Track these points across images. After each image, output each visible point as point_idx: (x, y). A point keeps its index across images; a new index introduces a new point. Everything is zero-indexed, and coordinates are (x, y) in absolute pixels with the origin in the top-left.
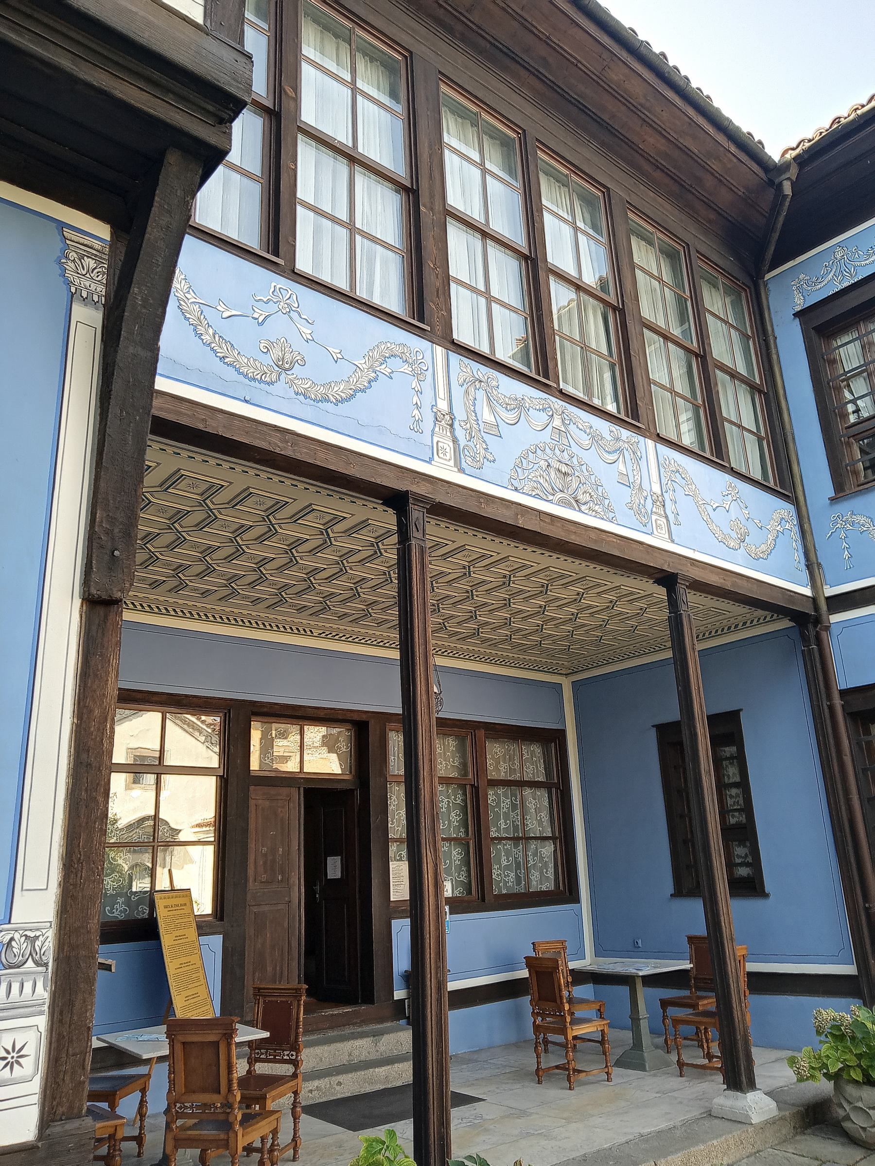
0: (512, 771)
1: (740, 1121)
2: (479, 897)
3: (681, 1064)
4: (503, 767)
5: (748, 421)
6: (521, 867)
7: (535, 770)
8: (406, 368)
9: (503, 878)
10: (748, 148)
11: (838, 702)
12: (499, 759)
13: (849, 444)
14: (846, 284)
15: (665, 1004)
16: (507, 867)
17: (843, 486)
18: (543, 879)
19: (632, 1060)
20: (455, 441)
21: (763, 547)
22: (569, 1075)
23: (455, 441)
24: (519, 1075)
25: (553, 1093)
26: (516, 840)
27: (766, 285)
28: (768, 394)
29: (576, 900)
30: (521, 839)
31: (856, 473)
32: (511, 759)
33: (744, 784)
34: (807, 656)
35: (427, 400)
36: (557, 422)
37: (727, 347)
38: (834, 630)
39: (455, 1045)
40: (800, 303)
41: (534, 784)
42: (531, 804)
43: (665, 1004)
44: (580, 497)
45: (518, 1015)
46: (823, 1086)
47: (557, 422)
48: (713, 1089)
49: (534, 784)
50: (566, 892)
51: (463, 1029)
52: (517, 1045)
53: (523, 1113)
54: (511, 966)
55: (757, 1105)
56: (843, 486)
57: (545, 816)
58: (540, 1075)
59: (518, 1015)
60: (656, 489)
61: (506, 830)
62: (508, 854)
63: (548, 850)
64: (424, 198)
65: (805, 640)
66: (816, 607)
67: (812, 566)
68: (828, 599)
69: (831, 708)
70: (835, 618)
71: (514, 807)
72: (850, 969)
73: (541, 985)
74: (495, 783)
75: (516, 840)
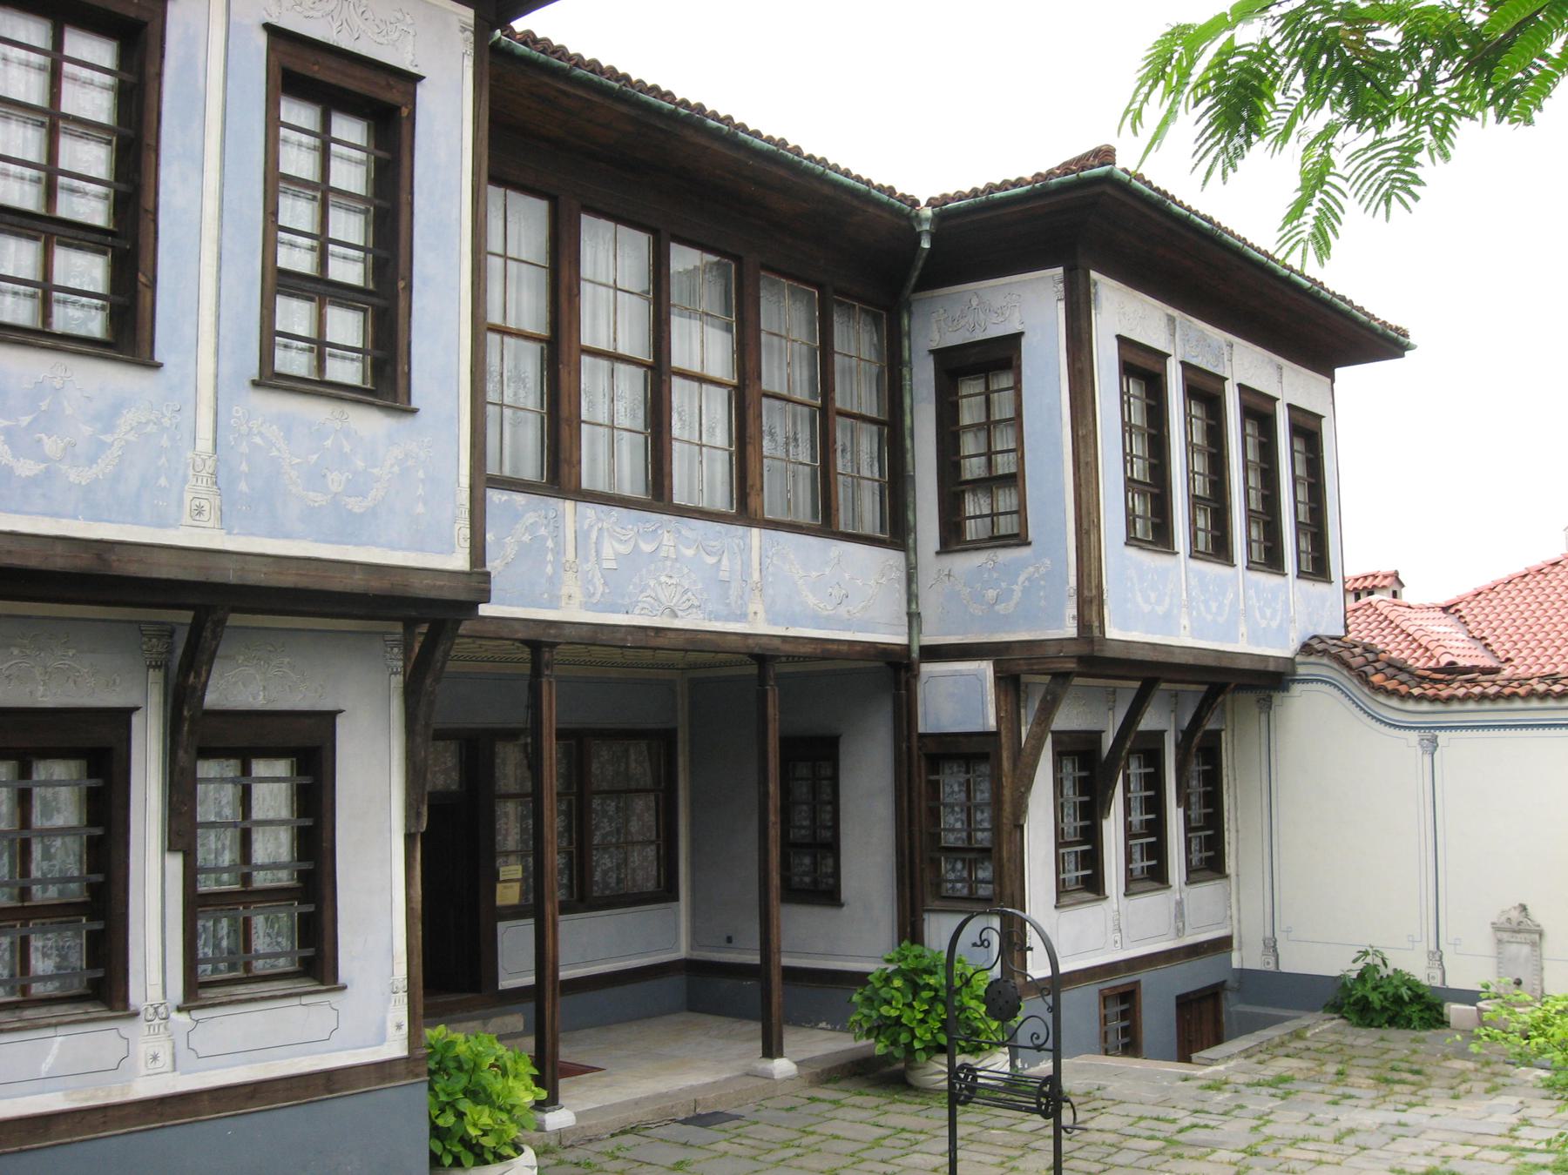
1: (768, 1077)
2: (583, 899)
17: (952, 538)
37: (857, 392)
55: (782, 1067)
56: (952, 538)
67: (913, 618)
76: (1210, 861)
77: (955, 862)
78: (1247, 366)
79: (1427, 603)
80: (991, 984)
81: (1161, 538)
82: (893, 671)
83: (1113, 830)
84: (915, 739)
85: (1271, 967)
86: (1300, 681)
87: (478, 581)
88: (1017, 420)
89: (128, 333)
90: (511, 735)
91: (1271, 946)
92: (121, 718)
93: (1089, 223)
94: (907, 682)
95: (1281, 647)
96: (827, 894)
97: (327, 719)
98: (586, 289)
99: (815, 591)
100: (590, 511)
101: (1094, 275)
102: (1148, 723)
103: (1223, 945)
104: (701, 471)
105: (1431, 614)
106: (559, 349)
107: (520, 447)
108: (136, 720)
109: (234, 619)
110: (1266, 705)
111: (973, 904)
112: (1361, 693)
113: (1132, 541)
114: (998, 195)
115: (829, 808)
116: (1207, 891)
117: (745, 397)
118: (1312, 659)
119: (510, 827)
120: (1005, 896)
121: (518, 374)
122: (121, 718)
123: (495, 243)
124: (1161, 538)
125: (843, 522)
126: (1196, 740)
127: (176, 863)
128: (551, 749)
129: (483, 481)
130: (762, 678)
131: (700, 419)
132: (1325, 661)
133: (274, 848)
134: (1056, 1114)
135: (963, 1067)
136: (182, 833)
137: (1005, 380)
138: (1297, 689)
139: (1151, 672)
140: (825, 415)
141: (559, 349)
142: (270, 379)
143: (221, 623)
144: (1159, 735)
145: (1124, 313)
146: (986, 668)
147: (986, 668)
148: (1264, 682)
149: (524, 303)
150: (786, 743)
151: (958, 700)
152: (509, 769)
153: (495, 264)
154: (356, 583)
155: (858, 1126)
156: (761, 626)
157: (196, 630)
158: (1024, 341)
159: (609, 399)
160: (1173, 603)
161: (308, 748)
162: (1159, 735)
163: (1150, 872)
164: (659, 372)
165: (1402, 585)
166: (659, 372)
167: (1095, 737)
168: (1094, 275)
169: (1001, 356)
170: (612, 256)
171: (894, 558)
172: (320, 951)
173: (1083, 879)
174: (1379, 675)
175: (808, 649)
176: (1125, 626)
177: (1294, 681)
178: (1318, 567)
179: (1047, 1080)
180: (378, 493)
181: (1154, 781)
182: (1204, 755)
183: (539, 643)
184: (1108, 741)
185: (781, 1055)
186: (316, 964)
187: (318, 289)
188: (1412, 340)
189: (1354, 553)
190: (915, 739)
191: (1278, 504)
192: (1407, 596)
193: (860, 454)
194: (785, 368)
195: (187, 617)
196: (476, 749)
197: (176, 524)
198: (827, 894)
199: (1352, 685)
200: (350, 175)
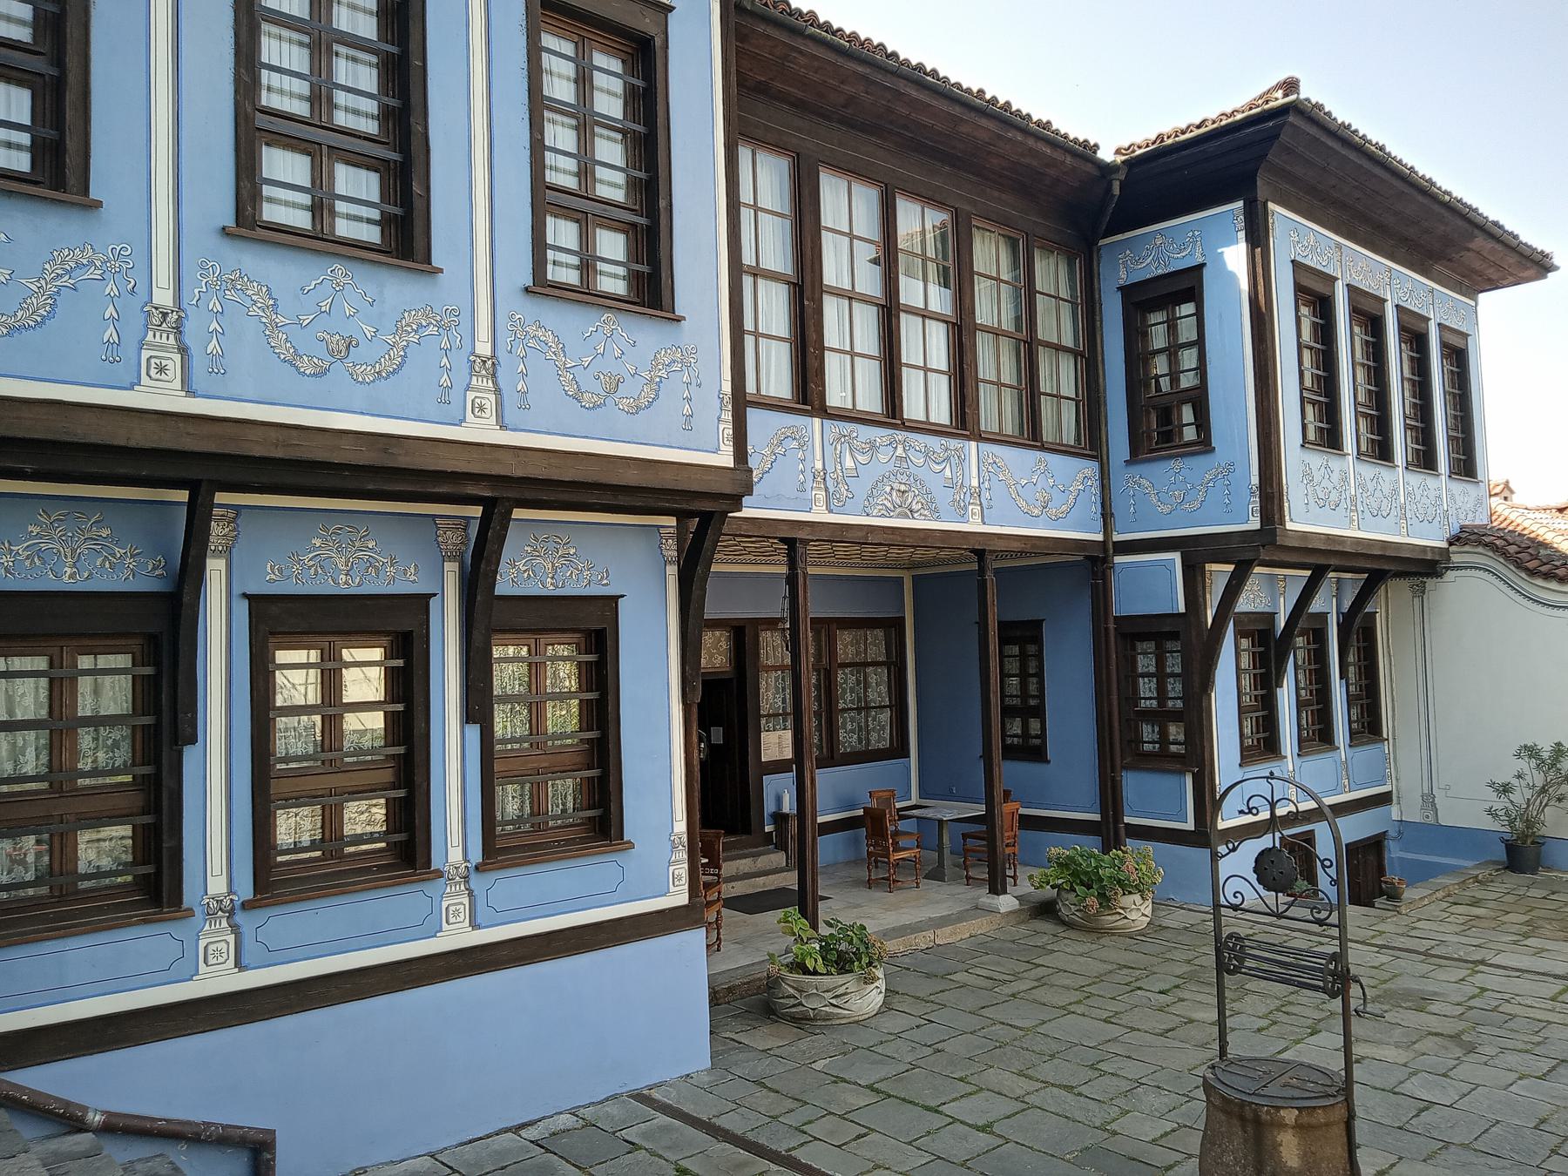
0: (858, 653)
1: (993, 911)
2: (832, 758)
3: (968, 878)
4: (851, 650)
5: (1068, 389)
6: (863, 731)
7: (877, 651)
8: (795, 444)
9: (848, 738)
10: (1084, 152)
11: (1112, 626)
12: (846, 645)
13: (1148, 413)
14: (1160, 272)
15: (965, 836)
16: (852, 731)
17: (1140, 450)
18: (881, 738)
19: (937, 875)
20: (827, 490)
21: (1064, 508)
22: (889, 884)
23: (827, 490)
24: (857, 883)
25: (878, 894)
26: (859, 709)
27: (1099, 249)
28: (1089, 360)
29: (907, 756)
30: (865, 708)
31: (1150, 438)
32: (858, 643)
33: (1040, 675)
34: (1094, 587)
35: (808, 464)
36: (900, 451)
37: (1056, 324)
38: (1118, 570)
39: (821, 860)
40: (1124, 278)
41: (875, 664)
42: (873, 679)
43: (965, 836)
44: (914, 507)
45: (856, 841)
46: (1049, 892)
47: (900, 451)
48: (984, 896)
49: (875, 664)
50: (899, 749)
51: (827, 849)
52: (856, 862)
53: (859, 906)
54: (852, 807)
55: (1006, 903)
56: (1140, 450)
57: (884, 689)
58: (870, 884)
59: (856, 841)
60: (975, 483)
61: (852, 702)
62: (852, 720)
63: (885, 716)
64: (807, 293)
65: (1094, 574)
66: (1105, 550)
67: (1107, 515)
68: (1115, 543)
69: (1107, 629)
70: (1118, 559)
71: (858, 683)
72: (1097, 817)
73: (871, 824)
74: (844, 665)
75: (859, 709)
76: (1368, 727)
77: (1150, 727)
78: (1399, 286)
79: (1543, 504)
80: (1262, 853)
81: (1330, 439)
82: (1092, 565)
83: (1286, 697)
84: (1111, 620)
85: (1431, 820)
86: (1453, 569)
87: (740, 481)
88: (1200, 343)
89: (405, 238)
90: (771, 623)
91: (1429, 801)
92: (420, 604)
93: (1269, 156)
94: (1104, 573)
95: (1431, 538)
96: (1034, 752)
97: (610, 603)
98: (827, 238)
99: (1018, 496)
100: (834, 427)
101: (1271, 205)
102: (1316, 606)
103: (1384, 799)
104: (927, 397)
105: (1547, 515)
106: (806, 292)
107: (774, 373)
108: (434, 604)
109: (518, 513)
110: (1421, 591)
111: (1162, 761)
112: (1520, 579)
113: (1305, 442)
114: (1183, 137)
115: (1034, 680)
116: (1367, 753)
117: (962, 332)
118: (1467, 548)
119: (772, 693)
120: (1197, 759)
121: (771, 309)
122: (420, 604)
123: (746, 195)
124: (1330, 439)
125: (1048, 434)
126: (1358, 620)
127: (474, 732)
128: (807, 636)
129: (741, 403)
130: (982, 570)
131: (925, 346)
132: (1480, 549)
133: (563, 718)
134: (1343, 993)
135: (1230, 936)
136: (478, 706)
137: (1188, 309)
138: (1450, 575)
139: (1320, 560)
140: (1028, 347)
141: (806, 292)
142: (541, 287)
143: (507, 517)
144: (1322, 617)
145: (1298, 237)
146: (1176, 557)
147: (1176, 557)
148: (1423, 568)
149: (771, 246)
150: (1003, 625)
151: (1151, 586)
152: (773, 648)
153: (746, 215)
154: (631, 478)
155: (1082, 959)
156: (974, 525)
157: (485, 521)
158: (1205, 271)
159: (848, 330)
160: (1342, 498)
161: (593, 629)
162: (1322, 617)
163: (1318, 735)
164: (890, 312)
165: (1512, 492)
166: (890, 312)
167: (1270, 617)
168: (1271, 205)
169: (1186, 286)
170: (846, 205)
171: (1090, 468)
172: (607, 811)
173: (1262, 744)
174: (1528, 560)
175: (1016, 546)
176: (1305, 517)
177: (1447, 569)
178: (1466, 466)
179: (1334, 957)
180: (654, 398)
181: (1320, 656)
182: (1359, 631)
183: (793, 542)
184: (1281, 622)
185: (1005, 892)
186: (601, 822)
187: (585, 211)
188: (1556, 261)
189: (1499, 450)
190: (1111, 620)
191: (1431, 412)
192: (1516, 499)
193: (1059, 376)
194: (993, 307)
195: (477, 511)
196: (742, 635)
197: (461, 422)
198: (1034, 752)
199: (1508, 571)
200: (609, 102)
